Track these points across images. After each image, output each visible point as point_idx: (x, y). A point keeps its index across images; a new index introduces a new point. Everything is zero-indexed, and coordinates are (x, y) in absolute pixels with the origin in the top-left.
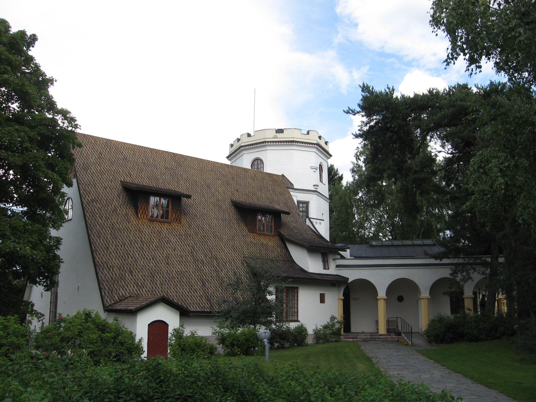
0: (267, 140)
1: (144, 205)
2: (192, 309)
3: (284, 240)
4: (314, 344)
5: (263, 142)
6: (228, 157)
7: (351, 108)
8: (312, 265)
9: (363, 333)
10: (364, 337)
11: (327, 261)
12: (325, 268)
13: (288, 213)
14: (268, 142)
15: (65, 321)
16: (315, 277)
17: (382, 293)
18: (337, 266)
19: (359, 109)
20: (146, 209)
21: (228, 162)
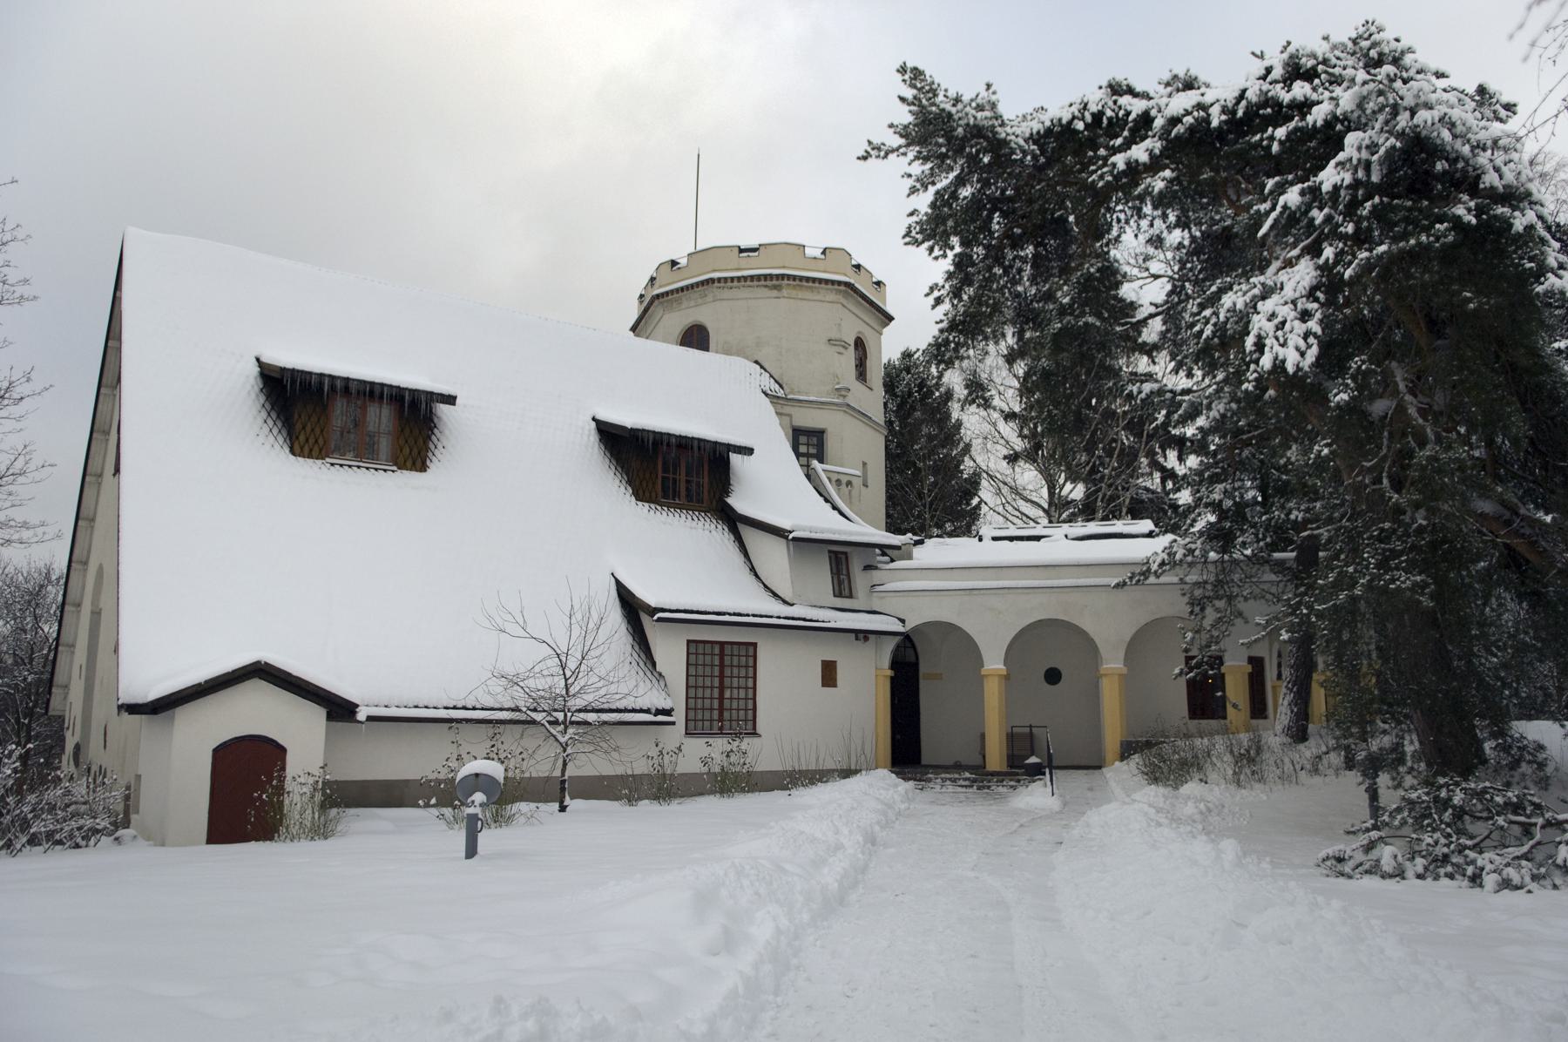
1: (314, 419)
6: (634, 329)
7: (876, 141)
11: (848, 575)
17: (994, 662)
19: (897, 141)
20: (318, 431)
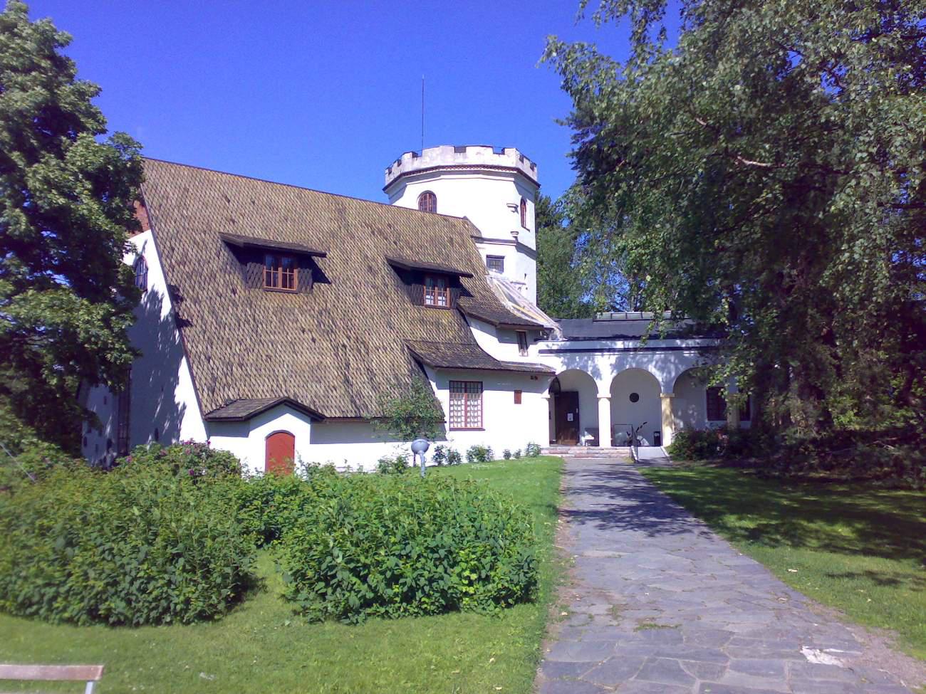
3: (466, 317)
4: (843, 669)
6: (384, 190)
8: (506, 353)
10: (578, 452)
13: (470, 276)
15: (316, 577)
18: (541, 352)
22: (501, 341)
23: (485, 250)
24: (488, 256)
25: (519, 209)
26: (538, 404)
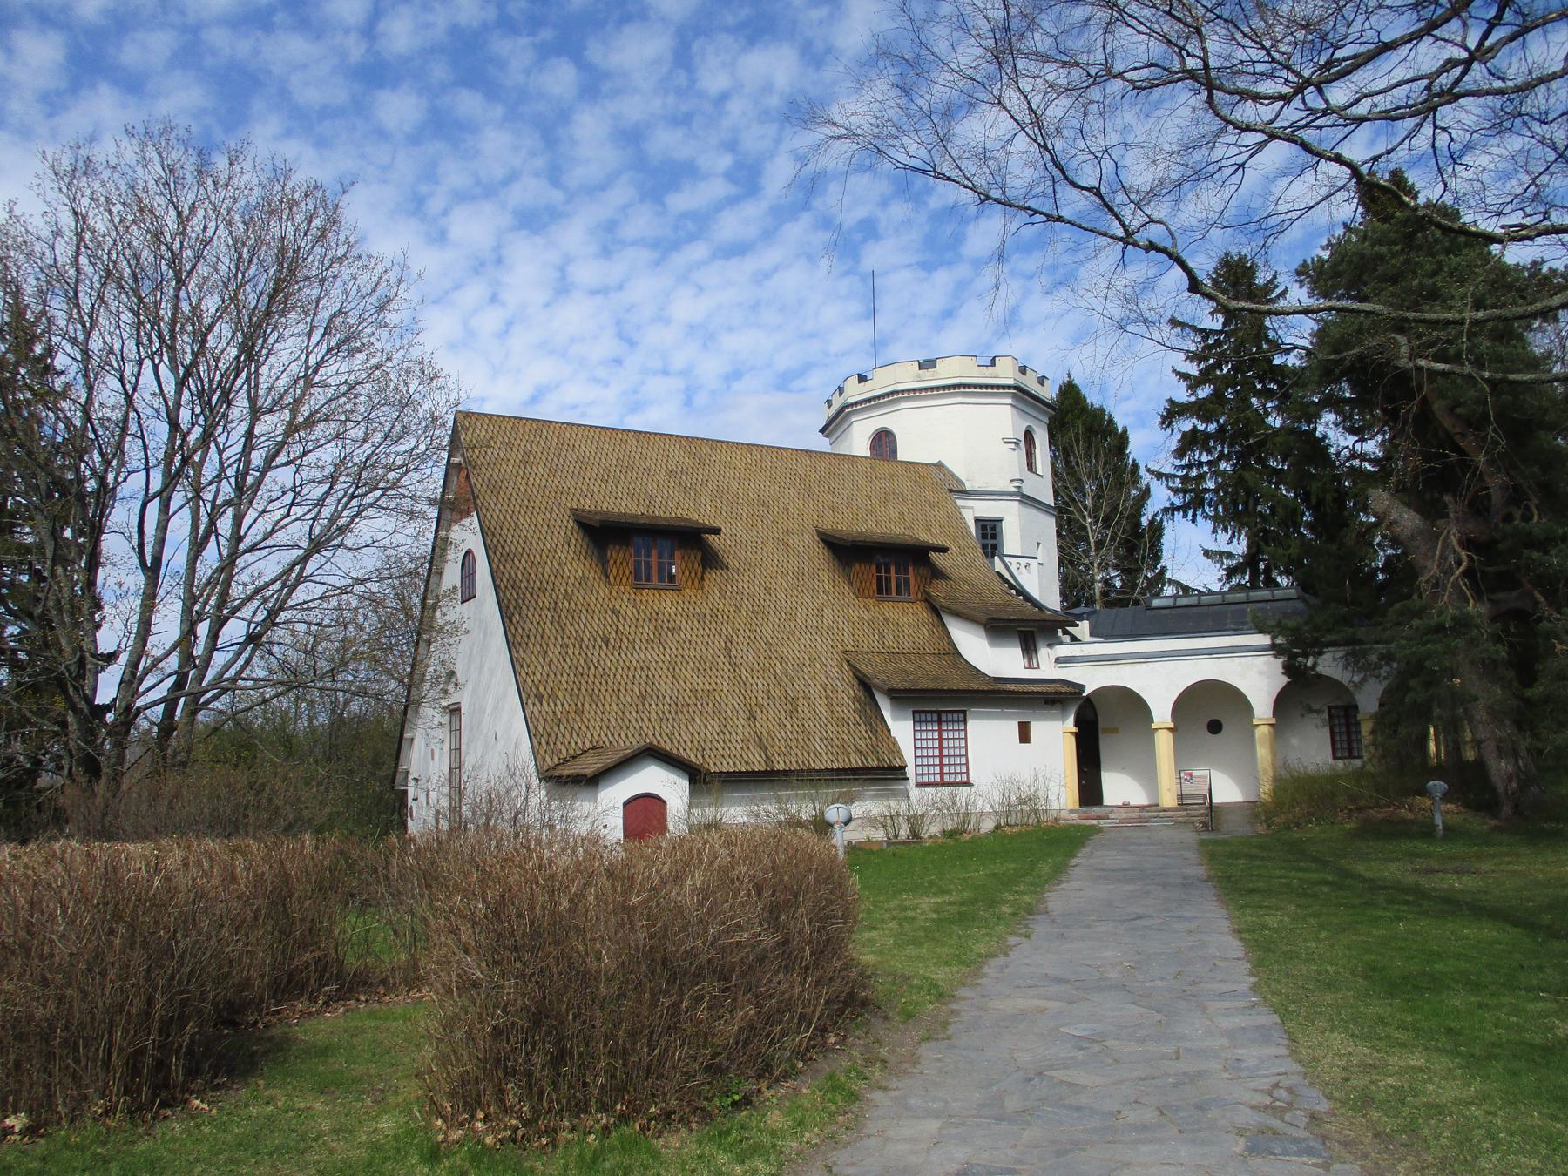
0: (901, 387)
2: (713, 769)
3: (936, 611)
5: (892, 393)
6: (822, 431)
8: (1000, 660)
9: (1126, 805)
12: (1030, 667)
13: (944, 550)
14: (903, 392)
16: (1012, 687)
17: (1162, 713)
21: (822, 444)
22: (992, 645)
23: (973, 510)
24: (977, 520)
25: (1023, 444)
26: (1056, 735)
